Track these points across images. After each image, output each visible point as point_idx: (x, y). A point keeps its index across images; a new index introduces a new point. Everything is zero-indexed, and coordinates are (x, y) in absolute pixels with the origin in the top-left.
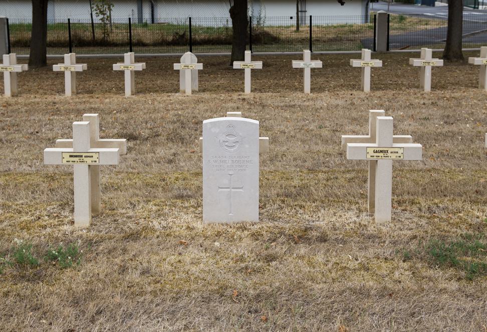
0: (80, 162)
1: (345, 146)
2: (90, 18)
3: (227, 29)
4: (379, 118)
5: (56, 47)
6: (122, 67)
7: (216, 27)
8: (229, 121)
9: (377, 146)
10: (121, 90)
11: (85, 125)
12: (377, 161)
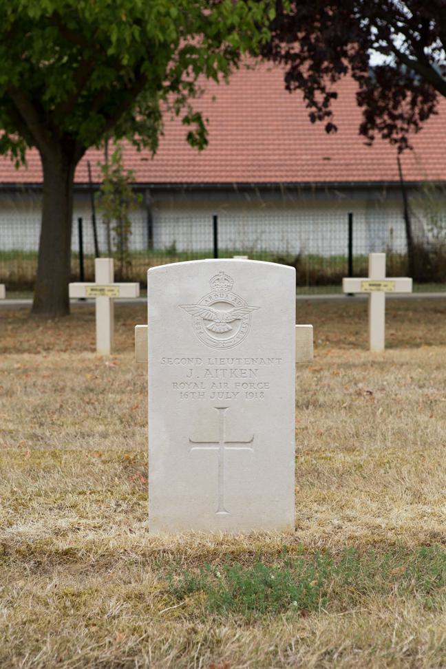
6: (366, 286)
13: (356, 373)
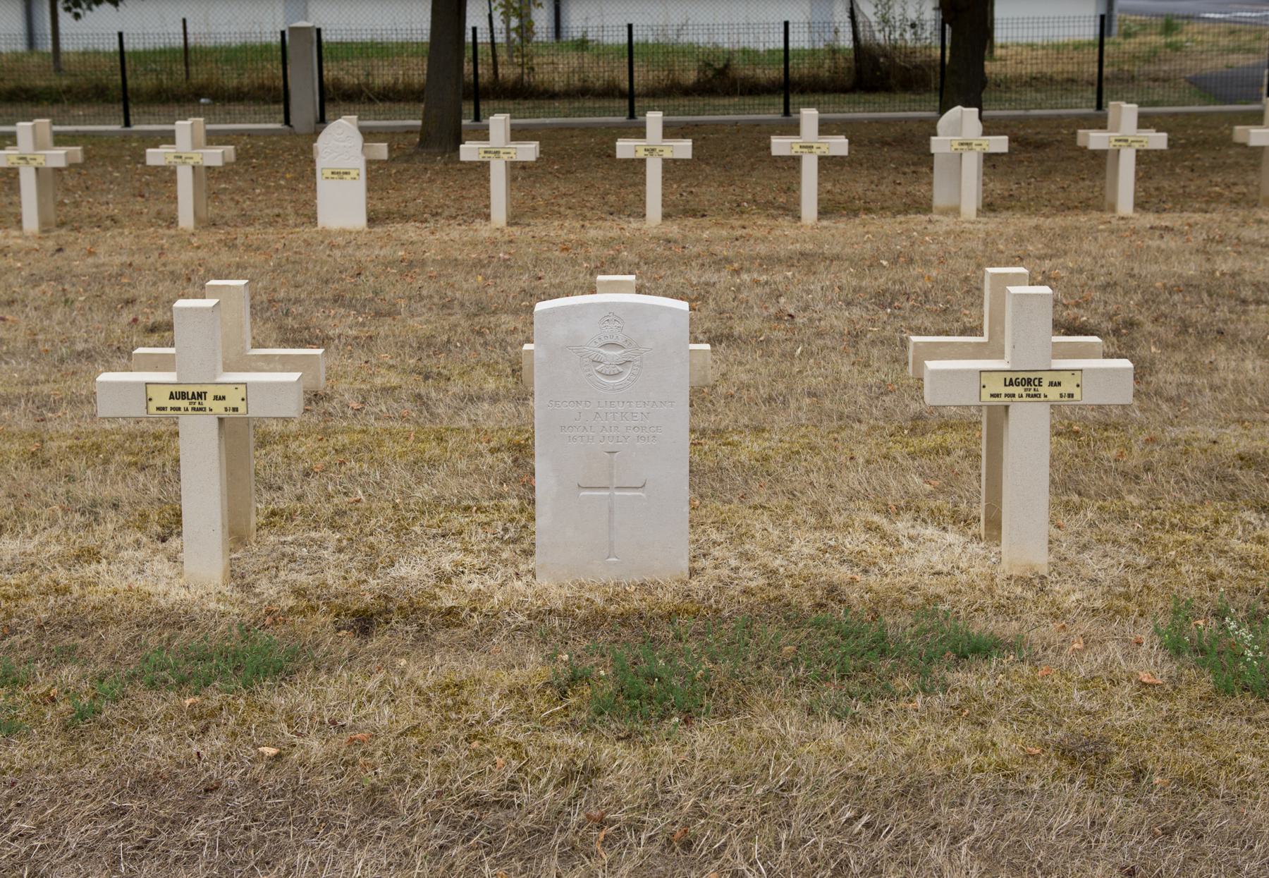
0: (194, 409)
1: (919, 366)
2: (181, 31)
3: (834, 52)
4: (1014, 290)
5: (400, 101)
6: (796, 148)
7: (761, 49)
8: (604, 305)
9: (1007, 367)
10: (1100, 202)
11: (207, 309)
12: (1007, 407)
13: (780, 276)
